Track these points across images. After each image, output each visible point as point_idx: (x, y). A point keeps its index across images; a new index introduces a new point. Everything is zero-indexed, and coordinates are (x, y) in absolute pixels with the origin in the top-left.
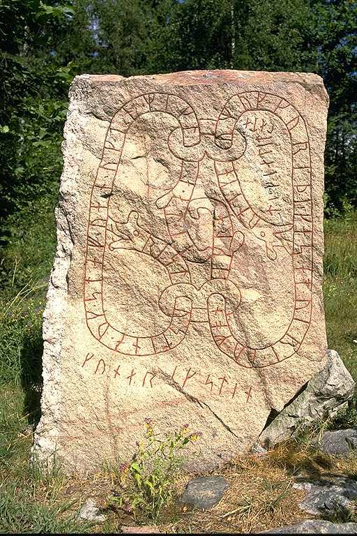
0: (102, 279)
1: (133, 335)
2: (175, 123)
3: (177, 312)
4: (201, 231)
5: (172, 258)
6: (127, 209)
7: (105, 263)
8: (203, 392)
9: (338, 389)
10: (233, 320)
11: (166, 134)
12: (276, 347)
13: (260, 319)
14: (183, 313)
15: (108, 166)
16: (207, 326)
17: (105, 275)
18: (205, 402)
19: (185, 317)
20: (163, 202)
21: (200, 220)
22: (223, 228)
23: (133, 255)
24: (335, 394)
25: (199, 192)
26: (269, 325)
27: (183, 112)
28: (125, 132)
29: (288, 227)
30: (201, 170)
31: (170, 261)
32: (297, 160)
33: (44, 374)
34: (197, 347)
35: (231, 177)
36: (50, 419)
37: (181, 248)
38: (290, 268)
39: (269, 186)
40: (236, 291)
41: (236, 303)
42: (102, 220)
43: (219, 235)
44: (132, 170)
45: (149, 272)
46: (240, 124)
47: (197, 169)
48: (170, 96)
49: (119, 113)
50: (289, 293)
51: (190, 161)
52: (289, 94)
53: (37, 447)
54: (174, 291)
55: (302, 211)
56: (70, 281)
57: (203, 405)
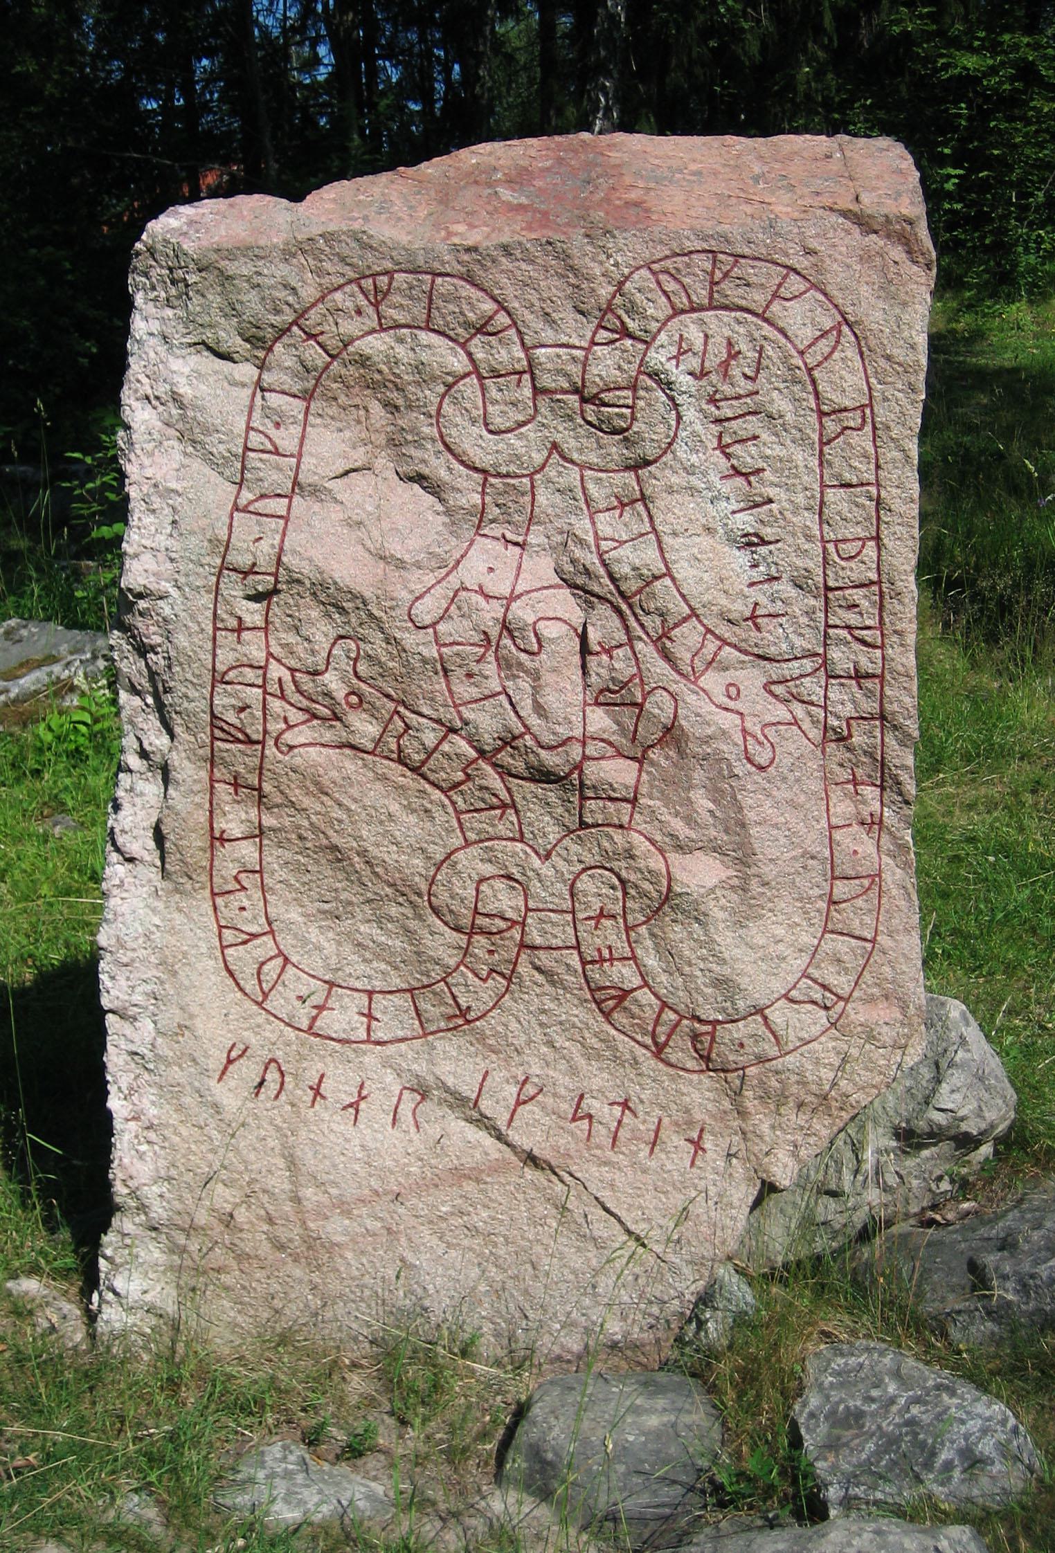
0: (261, 832)
1: (358, 985)
2: (458, 363)
3: (480, 921)
4: (548, 690)
5: (464, 770)
6: (322, 631)
7: (267, 787)
8: (563, 1141)
9: (962, 1119)
10: (649, 943)
11: (431, 396)
12: (775, 1015)
13: (725, 939)
14: (503, 925)
15: (259, 506)
16: (575, 961)
17: (268, 821)
18: (574, 1168)
19: (507, 935)
20: (427, 610)
21: (543, 656)
22: (613, 679)
23: (350, 765)
24: (953, 1132)
25: (541, 568)
26: (753, 956)
27: (483, 329)
28: (307, 396)
29: (808, 665)
30: (542, 499)
31: (460, 776)
32: (837, 462)
33: (114, 1103)
34: (543, 1018)
35: (634, 522)
36: (137, 1220)
37: (489, 742)
38: (816, 786)
39: (752, 542)
40: (657, 863)
41: (655, 894)
42: (251, 666)
43: (602, 699)
44: (336, 513)
45: (394, 807)
46: (659, 357)
47: (528, 498)
48: (439, 280)
49: (285, 339)
50: (813, 858)
51: (508, 475)
52: (809, 252)
53: (110, 1296)
54: (471, 862)
55: (852, 618)
56: (167, 845)
57: (567, 1178)
